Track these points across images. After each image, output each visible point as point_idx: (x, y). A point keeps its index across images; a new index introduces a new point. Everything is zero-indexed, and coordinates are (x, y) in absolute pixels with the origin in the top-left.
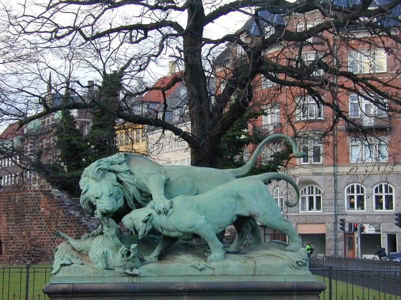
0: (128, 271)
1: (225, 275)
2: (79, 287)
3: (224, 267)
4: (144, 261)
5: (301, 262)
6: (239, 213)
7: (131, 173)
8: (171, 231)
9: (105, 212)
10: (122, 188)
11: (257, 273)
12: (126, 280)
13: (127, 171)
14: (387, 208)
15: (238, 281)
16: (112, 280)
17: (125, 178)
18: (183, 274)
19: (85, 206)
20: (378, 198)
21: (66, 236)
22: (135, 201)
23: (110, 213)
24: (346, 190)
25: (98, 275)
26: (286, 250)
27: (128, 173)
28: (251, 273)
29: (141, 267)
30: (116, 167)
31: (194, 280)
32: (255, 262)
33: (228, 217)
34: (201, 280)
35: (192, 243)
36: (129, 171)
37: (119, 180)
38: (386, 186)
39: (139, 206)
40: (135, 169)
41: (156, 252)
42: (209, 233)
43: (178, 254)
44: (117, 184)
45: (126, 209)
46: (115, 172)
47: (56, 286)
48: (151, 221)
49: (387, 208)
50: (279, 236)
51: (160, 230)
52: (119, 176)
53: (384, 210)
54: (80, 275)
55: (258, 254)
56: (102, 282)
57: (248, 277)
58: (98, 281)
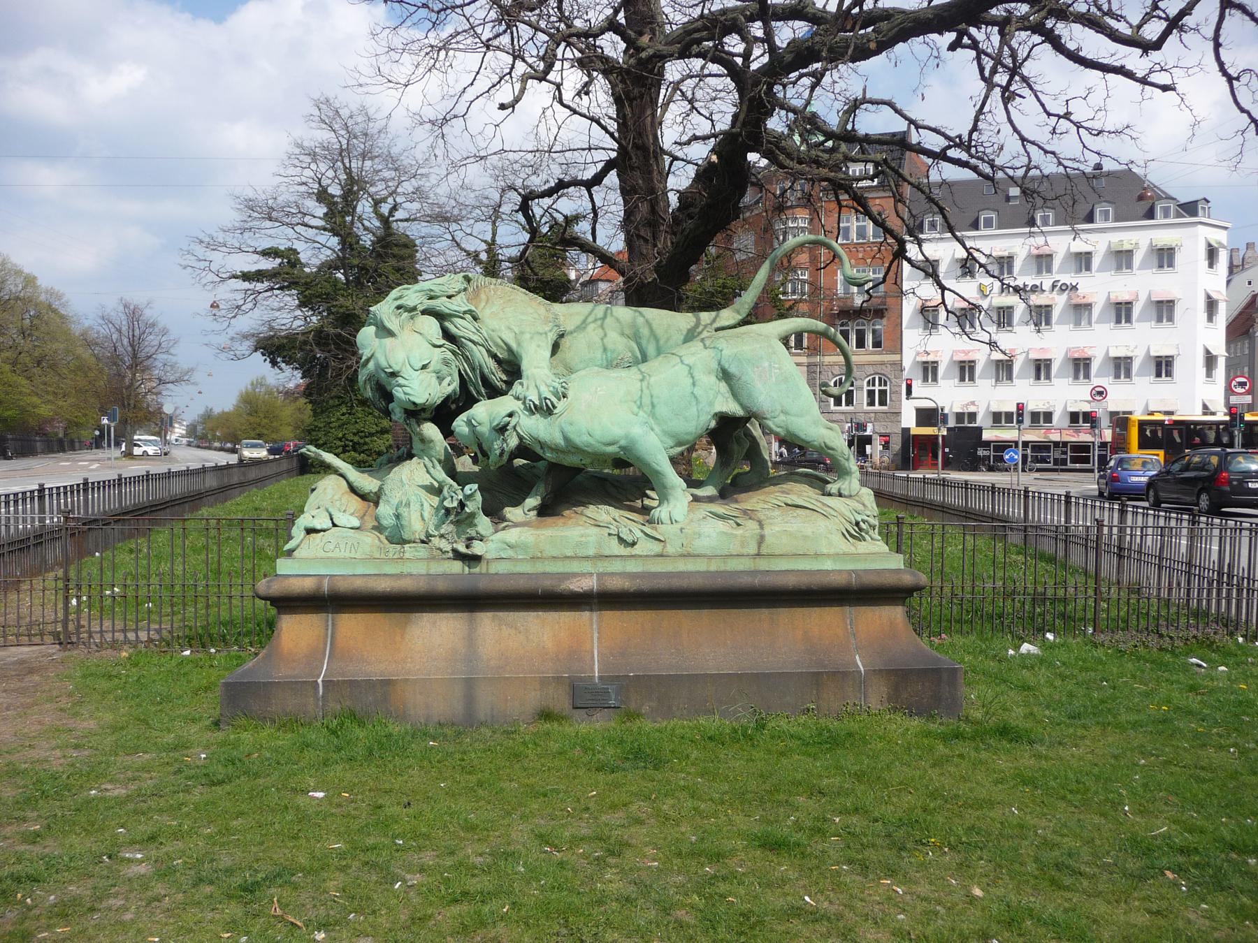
0: (462, 548)
1: (689, 555)
2: (344, 586)
3: (692, 532)
4: (503, 519)
5: (864, 521)
6: (724, 410)
7: (475, 319)
8: (563, 452)
9: (412, 408)
10: (453, 353)
11: (764, 551)
12: (457, 567)
13: (465, 313)
14: (881, 404)
15: (722, 568)
16: (420, 569)
17: (462, 327)
18: (591, 552)
19: (369, 393)
20: (871, 394)
21: (329, 457)
22: (486, 381)
23: (424, 410)
24: (865, 383)
25: (391, 555)
26: (830, 495)
27: (468, 316)
28: (752, 549)
29: (493, 537)
30: (442, 304)
31: (616, 567)
32: (761, 526)
33: (698, 420)
34: (633, 567)
35: (614, 480)
36: (470, 312)
37: (447, 335)
38: (880, 379)
39: (494, 392)
40: (485, 313)
41: (532, 502)
42: (656, 452)
43: (584, 504)
44: (443, 342)
45: (464, 399)
46: (440, 317)
47: (292, 580)
48: (514, 428)
49: (881, 404)
50: (808, 463)
51: (539, 451)
52: (447, 324)
53: (877, 407)
54: (347, 555)
55: (765, 502)
56: (398, 572)
57: (743, 560)
58: (389, 569)
